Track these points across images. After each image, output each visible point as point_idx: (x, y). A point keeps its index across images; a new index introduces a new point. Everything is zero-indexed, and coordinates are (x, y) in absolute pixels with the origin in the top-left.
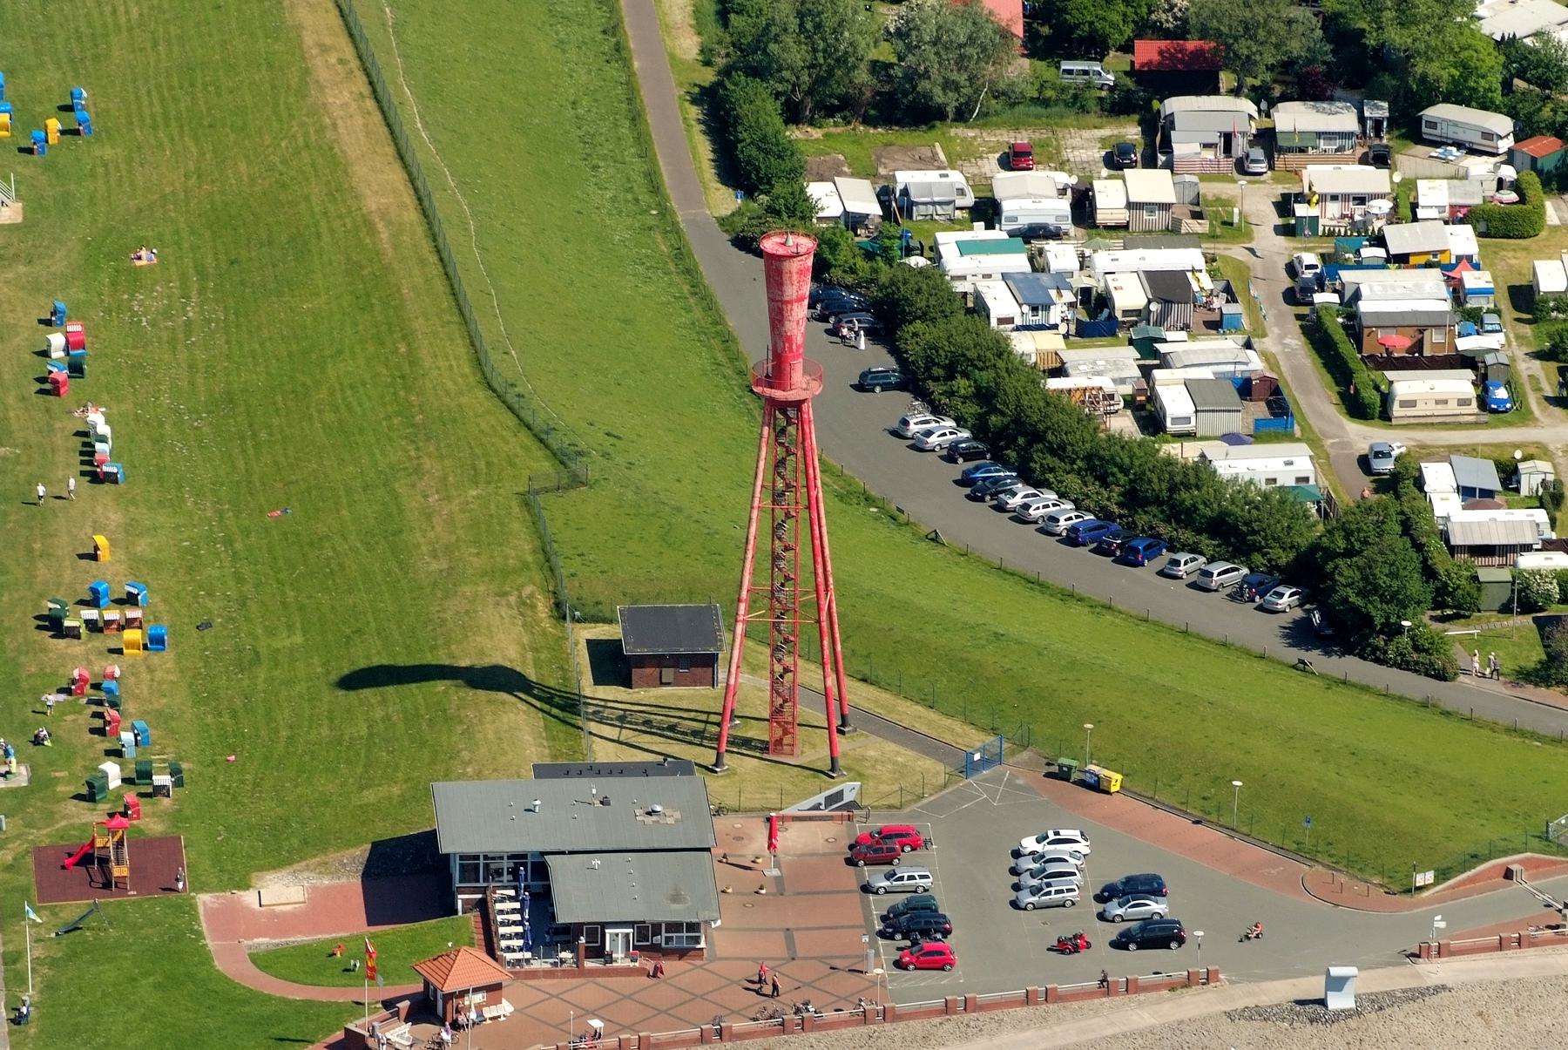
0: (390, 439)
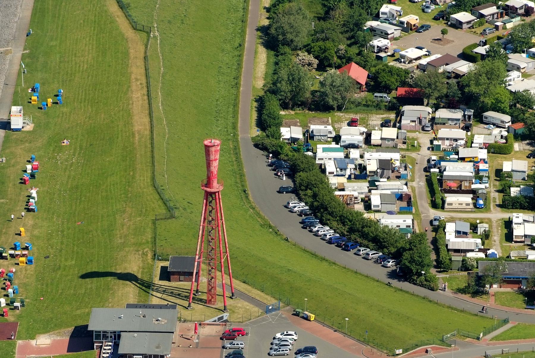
0: (119, 201)
